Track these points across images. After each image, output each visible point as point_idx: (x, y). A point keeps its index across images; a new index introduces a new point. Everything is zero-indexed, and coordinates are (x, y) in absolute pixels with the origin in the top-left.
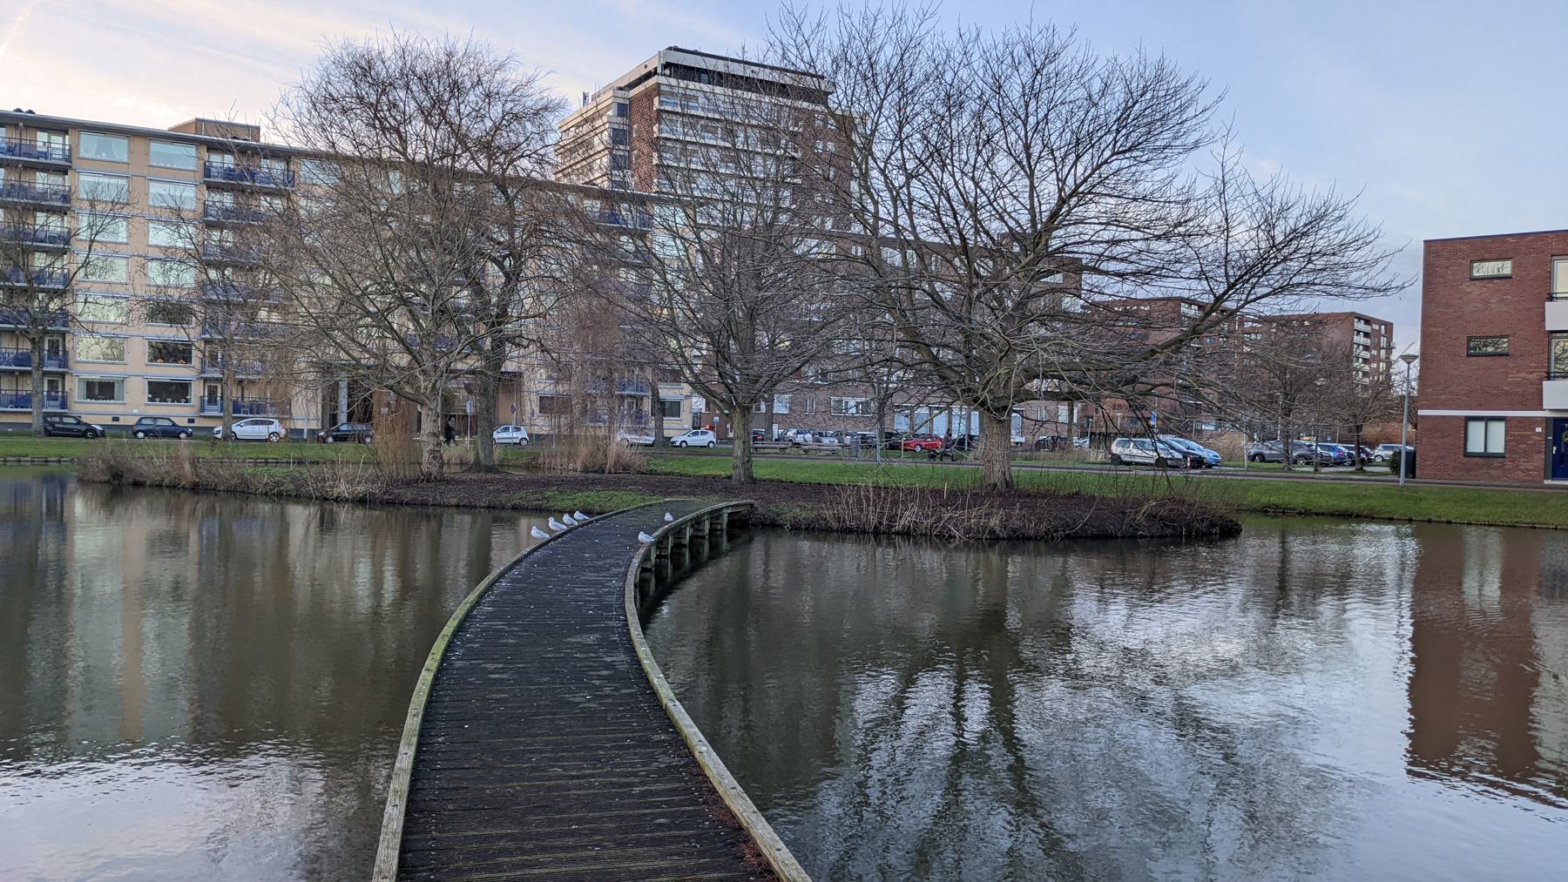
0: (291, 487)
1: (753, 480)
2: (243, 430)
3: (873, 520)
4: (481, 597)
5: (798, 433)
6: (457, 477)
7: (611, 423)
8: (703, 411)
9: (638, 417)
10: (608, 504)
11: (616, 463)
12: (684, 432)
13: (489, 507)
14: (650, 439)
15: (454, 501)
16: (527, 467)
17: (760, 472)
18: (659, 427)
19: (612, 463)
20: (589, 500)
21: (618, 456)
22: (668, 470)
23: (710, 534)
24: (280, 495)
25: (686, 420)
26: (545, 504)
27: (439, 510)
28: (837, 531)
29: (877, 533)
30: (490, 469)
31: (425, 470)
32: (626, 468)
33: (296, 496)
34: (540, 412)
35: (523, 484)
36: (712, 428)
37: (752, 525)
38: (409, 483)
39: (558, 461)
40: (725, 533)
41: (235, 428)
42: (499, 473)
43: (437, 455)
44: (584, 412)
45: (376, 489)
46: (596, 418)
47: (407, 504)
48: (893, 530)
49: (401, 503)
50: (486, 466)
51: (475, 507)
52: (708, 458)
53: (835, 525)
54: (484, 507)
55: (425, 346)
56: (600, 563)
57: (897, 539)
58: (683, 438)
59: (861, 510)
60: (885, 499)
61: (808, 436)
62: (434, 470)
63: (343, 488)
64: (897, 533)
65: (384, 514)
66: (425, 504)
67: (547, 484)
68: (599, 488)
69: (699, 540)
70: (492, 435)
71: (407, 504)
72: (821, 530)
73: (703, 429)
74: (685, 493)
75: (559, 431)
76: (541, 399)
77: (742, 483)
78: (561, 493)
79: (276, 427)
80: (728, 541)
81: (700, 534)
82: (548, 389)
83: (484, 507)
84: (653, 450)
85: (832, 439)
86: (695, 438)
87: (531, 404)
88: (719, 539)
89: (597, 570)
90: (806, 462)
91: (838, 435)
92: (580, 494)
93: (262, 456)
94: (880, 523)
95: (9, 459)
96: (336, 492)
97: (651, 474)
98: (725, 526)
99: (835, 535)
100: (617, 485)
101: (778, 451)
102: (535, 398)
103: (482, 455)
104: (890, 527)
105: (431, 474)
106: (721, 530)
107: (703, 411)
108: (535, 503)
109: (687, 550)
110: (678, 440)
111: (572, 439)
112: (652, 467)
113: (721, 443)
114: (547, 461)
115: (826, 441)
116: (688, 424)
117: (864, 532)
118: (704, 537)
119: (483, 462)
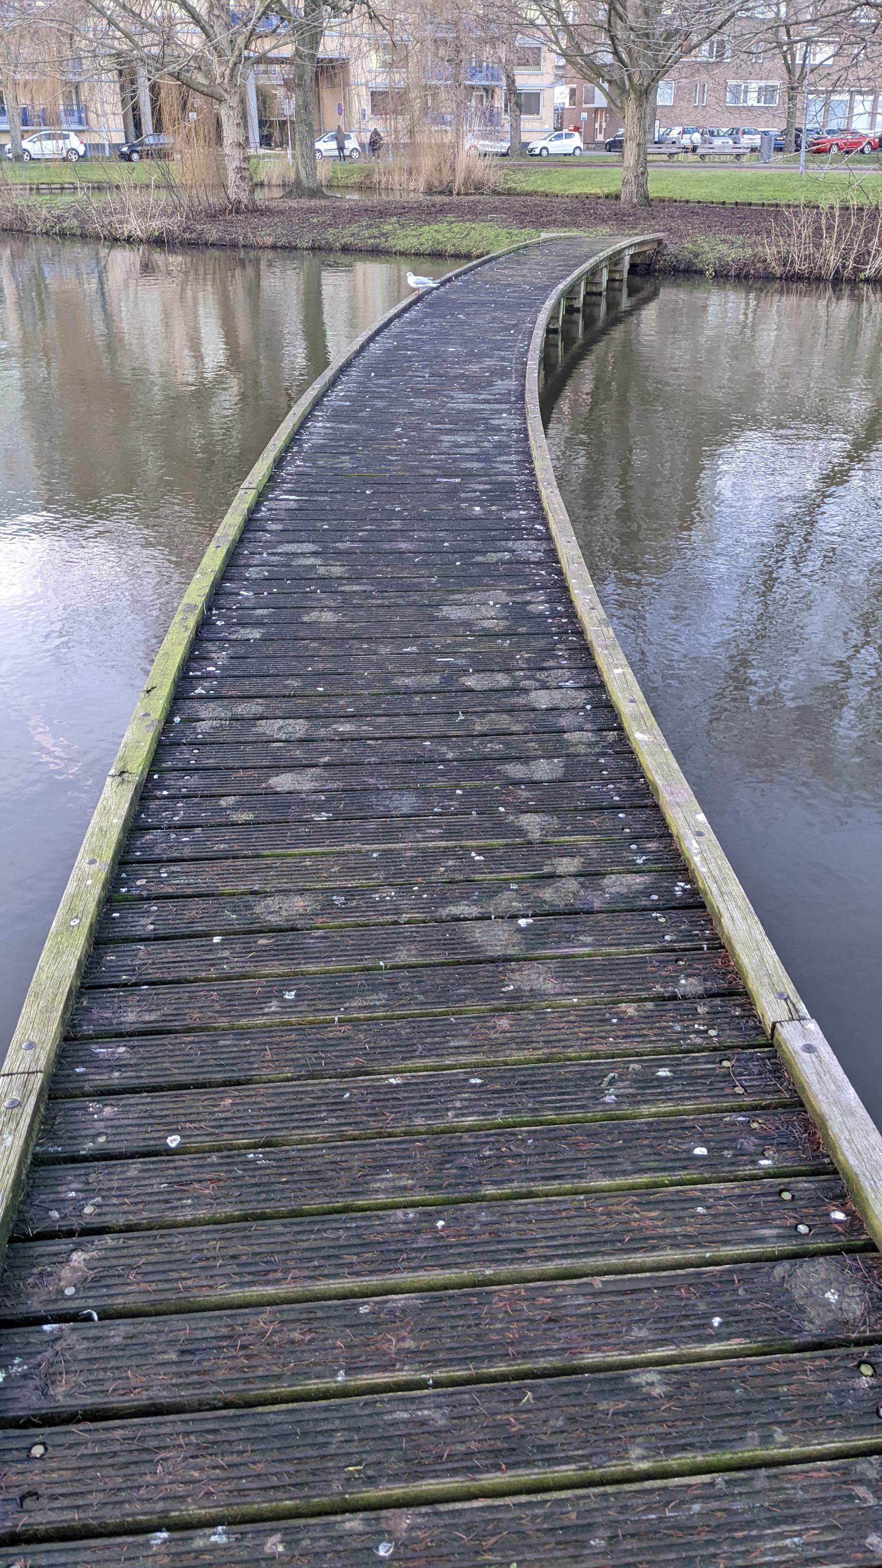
0: (75, 223)
1: (647, 201)
2: (32, 146)
3: (833, 260)
4: (279, 463)
5: (684, 132)
6: (274, 204)
7: (459, 124)
8: (567, 106)
9: (491, 118)
10: (464, 243)
11: (465, 184)
12: (544, 135)
13: (312, 249)
14: (504, 146)
15: (269, 241)
16: (360, 187)
17: (654, 189)
18: (516, 129)
19: (462, 180)
20: (439, 237)
21: (469, 171)
22: (529, 188)
23: (607, 289)
24: (62, 234)
25: (547, 118)
26: (382, 243)
27: (252, 254)
28: (781, 278)
29: (837, 281)
30: (315, 193)
31: (233, 197)
32: (479, 188)
33: (81, 235)
34: (373, 112)
35: (355, 213)
36: (577, 129)
37: (660, 271)
38: (214, 215)
39: (397, 178)
40: (625, 284)
41: (26, 144)
42: (326, 197)
43: (246, 174)
44: (425, 110)
45: (172, 224)
46: (440, 120)
47: (213, 245)
48: (862, 276)
49: (206, 244)
50: (310, 189)
51: (296, 248)
52: (580, 169)
53: (778, 270)
54: (307, 249)
55: (216, 12)
56: (475, 368)
57: (865, 289)
58: (545, 143)
59: (817, 246)
60: (857, 228)
61: (697, 137)
62: (244, 197)
63: (134, 223)
64: (867, 280)
65: (188, 259)
66: (234, 246)
67: (383, 213)
68: (450, 217)
69: (594, 298)
70: (313, 145)
71: (213, 245)
72: (757, 278)
73: (565, 131)
74: (564, 224)
75: (396, 138)
76: (373, 93)
77: (634, 206)
78: (403, 226)
79: (74, 142)
80: (630, 295)
81: (594, 289)
82: (381, 82)
83: (307, 249)
84: (506, 161)
85: (726, 140)
86: (558, 142)
87: (361, 102)
88: (617, 294)
89: (474, 384)
90: (704, 173)
91: (734, 133)
92: (426, 228)
93: (56, 180)
94: (844, 267)
95: (42, 186)
96: (126, 230)
97: (509, 194)
98: (626, 275)
99: (777, 285)
100: (473, 213)
101: (665, 157)
102: (365, 93)
103: (303, 174)
104: (857, 271)
105: (240, 202)
106: (621, 280)
107: (567, 106)
108: (371, 241)
109: (581, 315)
110: (537, 145)
111: (413, 148)
112: (511, 184)
113: (588, 149)
114: (384, 180)
115: (717, 142)
116: (549, 125)
117: (819, 279)
118: (600, 294)
119: (306, 183)
